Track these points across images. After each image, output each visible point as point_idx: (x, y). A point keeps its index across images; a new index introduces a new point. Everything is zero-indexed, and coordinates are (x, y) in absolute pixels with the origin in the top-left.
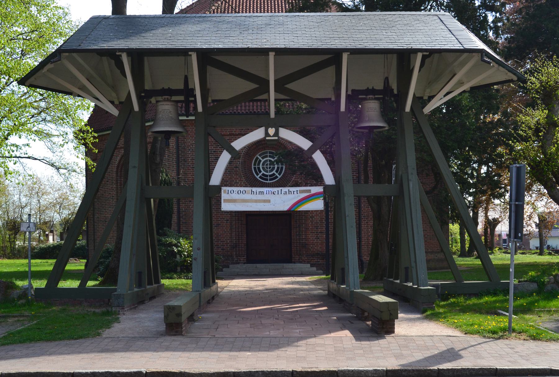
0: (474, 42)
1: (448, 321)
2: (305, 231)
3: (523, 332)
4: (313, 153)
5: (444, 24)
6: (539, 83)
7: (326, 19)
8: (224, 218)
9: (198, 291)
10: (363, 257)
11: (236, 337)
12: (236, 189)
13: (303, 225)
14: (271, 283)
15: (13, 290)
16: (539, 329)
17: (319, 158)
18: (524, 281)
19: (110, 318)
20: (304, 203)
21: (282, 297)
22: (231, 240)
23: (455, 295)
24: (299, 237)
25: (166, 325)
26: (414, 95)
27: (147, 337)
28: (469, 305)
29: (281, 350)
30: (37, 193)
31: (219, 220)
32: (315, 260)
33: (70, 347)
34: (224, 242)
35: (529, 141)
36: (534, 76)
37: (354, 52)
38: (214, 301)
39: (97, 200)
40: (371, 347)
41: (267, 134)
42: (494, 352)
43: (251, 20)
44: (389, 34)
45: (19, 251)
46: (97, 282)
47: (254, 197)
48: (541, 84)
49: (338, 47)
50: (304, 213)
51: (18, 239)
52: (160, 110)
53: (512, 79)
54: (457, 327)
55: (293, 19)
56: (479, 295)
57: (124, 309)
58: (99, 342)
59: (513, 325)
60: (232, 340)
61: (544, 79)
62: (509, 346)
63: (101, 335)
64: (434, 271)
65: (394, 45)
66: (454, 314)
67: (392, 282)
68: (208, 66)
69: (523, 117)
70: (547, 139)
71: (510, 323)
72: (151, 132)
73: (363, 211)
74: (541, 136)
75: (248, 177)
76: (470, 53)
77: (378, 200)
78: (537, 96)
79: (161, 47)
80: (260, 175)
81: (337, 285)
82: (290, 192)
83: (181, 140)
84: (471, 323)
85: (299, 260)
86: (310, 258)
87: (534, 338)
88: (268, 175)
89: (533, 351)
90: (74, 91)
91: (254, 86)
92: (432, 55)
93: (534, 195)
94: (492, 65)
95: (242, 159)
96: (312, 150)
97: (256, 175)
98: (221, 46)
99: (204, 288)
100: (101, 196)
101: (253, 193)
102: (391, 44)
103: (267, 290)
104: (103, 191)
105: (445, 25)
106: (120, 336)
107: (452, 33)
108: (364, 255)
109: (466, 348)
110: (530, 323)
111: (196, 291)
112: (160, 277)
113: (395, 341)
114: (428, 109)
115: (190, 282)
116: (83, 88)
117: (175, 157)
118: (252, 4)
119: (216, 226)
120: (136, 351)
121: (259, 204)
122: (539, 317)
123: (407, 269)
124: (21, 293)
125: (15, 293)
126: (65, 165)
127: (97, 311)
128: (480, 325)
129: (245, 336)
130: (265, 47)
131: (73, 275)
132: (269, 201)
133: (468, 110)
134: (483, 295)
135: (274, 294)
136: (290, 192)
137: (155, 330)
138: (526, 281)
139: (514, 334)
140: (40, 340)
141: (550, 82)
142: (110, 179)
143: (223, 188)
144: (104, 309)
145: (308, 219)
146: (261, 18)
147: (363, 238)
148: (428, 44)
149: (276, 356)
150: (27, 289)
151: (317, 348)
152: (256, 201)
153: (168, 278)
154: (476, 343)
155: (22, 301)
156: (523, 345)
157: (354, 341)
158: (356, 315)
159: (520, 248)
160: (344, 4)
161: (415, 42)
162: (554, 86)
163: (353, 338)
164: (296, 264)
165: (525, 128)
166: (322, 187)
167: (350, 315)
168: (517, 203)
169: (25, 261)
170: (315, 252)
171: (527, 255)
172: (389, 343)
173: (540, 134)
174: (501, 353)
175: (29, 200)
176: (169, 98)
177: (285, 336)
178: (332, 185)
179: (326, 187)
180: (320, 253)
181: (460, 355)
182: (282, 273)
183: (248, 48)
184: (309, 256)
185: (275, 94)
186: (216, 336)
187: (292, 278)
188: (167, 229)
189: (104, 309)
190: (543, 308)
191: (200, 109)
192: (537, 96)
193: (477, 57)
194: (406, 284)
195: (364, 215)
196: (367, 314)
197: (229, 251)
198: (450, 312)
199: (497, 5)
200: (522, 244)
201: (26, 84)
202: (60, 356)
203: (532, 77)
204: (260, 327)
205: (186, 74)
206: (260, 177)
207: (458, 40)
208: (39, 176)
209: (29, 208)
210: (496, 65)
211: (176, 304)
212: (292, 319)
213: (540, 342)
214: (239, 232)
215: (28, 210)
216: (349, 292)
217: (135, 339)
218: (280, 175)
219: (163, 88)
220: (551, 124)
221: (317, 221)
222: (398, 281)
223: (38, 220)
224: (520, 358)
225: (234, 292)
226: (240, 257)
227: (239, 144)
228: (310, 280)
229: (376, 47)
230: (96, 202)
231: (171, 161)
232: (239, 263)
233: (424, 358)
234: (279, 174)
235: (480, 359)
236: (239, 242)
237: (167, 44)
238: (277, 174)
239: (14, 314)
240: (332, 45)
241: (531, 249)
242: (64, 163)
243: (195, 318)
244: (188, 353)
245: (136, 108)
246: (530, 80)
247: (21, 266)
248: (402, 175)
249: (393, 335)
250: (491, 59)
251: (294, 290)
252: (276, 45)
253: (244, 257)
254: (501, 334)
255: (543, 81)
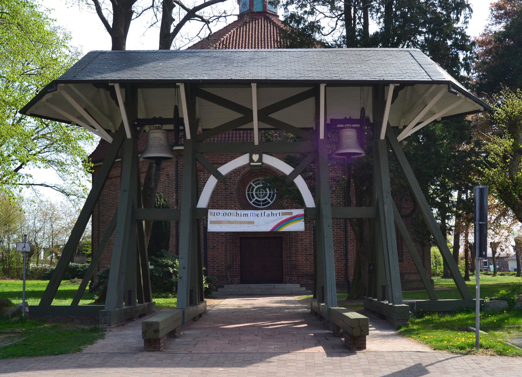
0: (442, 75)
1: (419, 337)
2: (295, 253)
3: (490, 347)
4: (295, 178)
5: (414, 58)
6: (505, 114)
7: (306, 54)
8: (220, 241)
9: (183, 309)
10: (350, 277)
11: (212, 353)
12: (222, 211)
13: (293, 248)
14: (261, 302)
15: (8, 308)
16: (507, 345)
17: (300, 182)
18: (495, 299)
19: (96, 334)
20: (284, 225)
21: (267, 315)
22: (226, 261)
23: (430, 312)
24: (290, 259)
25: (144, 341)
26: (388, 123)
27: (126, 353)
28: (443, 322)
29: (253, 365)
30: (51, 218)
31: (215, 243)
32: (305, 280)
33: (49, 363)
34: (219, 263)
35: (497, 167)
36: (500, 108)
37: (331, 84)
38: (201, 319)
39: (102, 224)
40: (341, 363)
41: (251, 160)
42: (460, 367)
43: (237, 55)
44: (364, 67)
45: (32, 272)
46: (94, 301)
47: (239, 219)
48: (507, 114)
49: (315, 79)
50: (295, 236)
51: (32, 261)
52: (151, 137)
53: (479, 110)
54: (427, 343)
55: (276, 54)
56: (452, 313)
57: (110, 326)
58: (78, 358)
59: (480, 341)
60: (207, 355)
61: (509, 109)
62: (476, 362)
63: (82, 351)
64: (416, 291)
65: (367, 77)
66: (427, 330)
67: (371, 301)
68: (197, 98)
69: (492, 145)
70: (514, 165)
71: (477, 338)
72: (143, 158)
73: (349, 234)
74: (508, 163)
75: (242, 202)
76: (438, 84)
77: (360, 223)
78: (503, 126)
79: (150, 78)
80: (254, 200)
81: (318, 303)
82: (273, 215)
83: (180, 168)
84: (440, 339)
85: (290, 280)
86: (300, 278)
87: (501, 354)
88: (260, 201)
89: (498, 366)
90: (73, 120)
91: (239, 115)
92: (405, 89)
93: (509, 220)
94: (458, 95)
95: (236, 186)
96: (293, 175)
97: (249, 201)
98: (206, 78)
99: (190, 305)
100: (106, 220)
101: (238, 215)
102: (365, 76)
103: (254, 308)
104: (108, 215)
105: (415, 60)
106: (100, 352)
107: (421, 66)
108: (351, 276)
109: (433, 364)
110: (498, 339)
111: (181, 309)
112: (151, 295)
113: (365, 357)
114: (401, 137)
115: (174, 300)
116: (81, 118)
117: (174, 183)
118: (247, 45)
119: (212, 249)
120: (112, 366)
121: (243, 225)
122: (508, 333)
123: (384, 287)
124: (15, 311)
125: (10, 311)
126: (74, 192)
127: (86, 327)
128: (449, 341)
129: (220, 352)
130: (248, 78)
131: (65, 295)
132: (253, 223)
133: (442, 140)
134: (456, 312)
135: (260, 312)
136: (273, 215)
137: (136, 345)
138: (497, 299)
139: (481, 350)
140: (23, 355)
141: (514, 112)
142: (115, 205)
143: (210, 211)
144: (93, 326)
145: (298, 242)
146: (246, 53)
147: (350, 260)
148: (399, 76)
149: (247, 372)
150: (22, 306)
151: (289, 364)
152: (241, 223)
153: (163, 297)
154: (443, 359)
155: (16, 318)
156: (489, 360)
157: (325, 357)
158: (333, 331)
159: (499, 270)
160: (327, 43)
161: (387, 74)
162: (519, 116)
163: (325, 353)
164: (287, 284)
165: (494, 155)
166: (303, 210)
167: (328, 331)
168: (481, 223)
169: (21, 282)
170: (304, 273)
171: (506, 276)
172: (359, 358)
173: (507, 161)
174: (467, 368)
175: (43, 224)
176: (160, 127)
177: (259, 352)
178: (313, 208)
179: (307, 210)
180: (310, 274)
181: (427, 371)
182: (273, 293)
183: (231, 80)
184: (299, 277)
185: (258, 122)
186: (193, 352)
187: (282, 297)
188: (164, 251)
189: (93, 326)
190: (512, 325)
191: (188, 136)
192: (503, 126)
193: (445, 89)
194: (383, 302)
195: (351, 238)
196: (342, 331)
197: (224, 272)
198: (424, 329)
199: (467, 45)
200: (502, 267)
201: (27, 113)
202: (37, 372)
203: (498, 108)
204: (238, 343)
205: (177, 104)
206: (254, 203)
207: (426, 73)
208: (53, 203)
209: (43, 232)
210: (463, 97)
211: (154, 321)
212: (271, 336)
213: (506, 358)
214: (233, 254)
215: (41, 234)
216: (326, 310)
217: (113, 354)
218: (272, 201)
219: (155, 117)
220: (517, 151)
221: (307, 244)
222: (376, 300)
223: (51, 244)
224: (485, 373)
225: (223, 310)
226: (234, 277)
227: (225, 169)
228: (298, 300)
229: (350, 79)
230: (101, 226)
231: (170, 188)
232: (233, 284)
233: (391, 373)
234: (271, 200)
235: (446, 374)
236: (233, 263)
237: (156, 75)
238: (269, 200)
239: (6, 331)
240: (310, 77)
241: (509, 271)
242: (74, 190)
243: (176, 334)
244: (162, 368)
245: (129, 135)
246: (497, 110)
247: (31, 286)
248: (378, 198)
249: (364, 351)
250: (457, 90)
251: (280, 308)
252: (258, 77)
253: (238, 277)
254: (468, 350)
255: (508, 111)
